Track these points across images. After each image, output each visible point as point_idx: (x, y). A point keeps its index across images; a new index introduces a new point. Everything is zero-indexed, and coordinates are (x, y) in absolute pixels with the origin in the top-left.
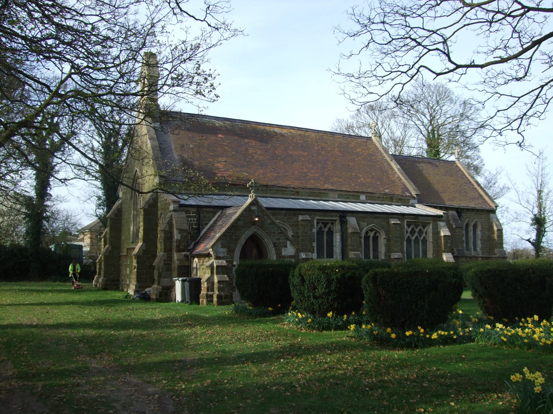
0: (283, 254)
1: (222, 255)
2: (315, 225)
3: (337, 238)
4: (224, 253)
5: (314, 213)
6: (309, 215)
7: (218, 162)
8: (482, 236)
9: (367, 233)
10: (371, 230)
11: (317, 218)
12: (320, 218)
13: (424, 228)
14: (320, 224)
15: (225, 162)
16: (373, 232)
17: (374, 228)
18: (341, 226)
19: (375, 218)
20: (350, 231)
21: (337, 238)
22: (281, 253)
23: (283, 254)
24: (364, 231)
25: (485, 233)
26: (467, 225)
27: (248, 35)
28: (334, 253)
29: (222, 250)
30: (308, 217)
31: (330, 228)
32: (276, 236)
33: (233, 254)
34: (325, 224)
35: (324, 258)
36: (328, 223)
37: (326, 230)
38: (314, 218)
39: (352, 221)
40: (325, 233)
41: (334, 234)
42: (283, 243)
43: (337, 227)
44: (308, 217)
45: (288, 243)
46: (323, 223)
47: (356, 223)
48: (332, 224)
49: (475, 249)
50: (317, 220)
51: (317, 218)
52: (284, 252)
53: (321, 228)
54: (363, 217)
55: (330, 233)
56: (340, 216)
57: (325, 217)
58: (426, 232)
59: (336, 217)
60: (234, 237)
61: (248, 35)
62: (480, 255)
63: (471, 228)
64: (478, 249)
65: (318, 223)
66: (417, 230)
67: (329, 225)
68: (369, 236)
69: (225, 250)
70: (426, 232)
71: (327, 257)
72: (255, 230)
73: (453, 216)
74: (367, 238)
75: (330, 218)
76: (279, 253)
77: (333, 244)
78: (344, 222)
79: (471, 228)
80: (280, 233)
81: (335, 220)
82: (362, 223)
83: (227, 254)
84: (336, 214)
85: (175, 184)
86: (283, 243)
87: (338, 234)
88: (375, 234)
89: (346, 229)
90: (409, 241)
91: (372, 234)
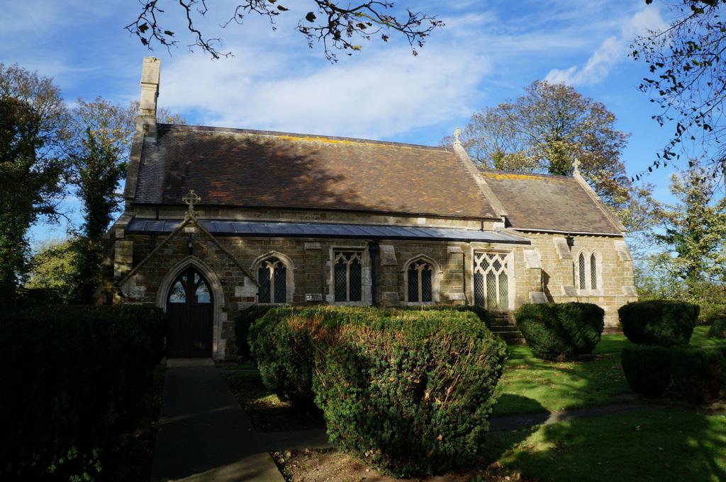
0: (237, 294)
1: (136, 296)
2: (331, 257)
3: (366, 274)
4: (140, 293)
5: (330, 240)
6: (320, 242)
8: (604, 270)
9: (413, 266)
10: (420, 262)
11: (332, 246)
12: (338, 247)
13: (503, 258)
16: (423, 266)
17: (422, 258)
19: (425, 245)
20: (384, 262)
21: (366, 274)
22: (234, 294)
23: (237, 294)
25: (608, 266)
27: (653, 118)
28: (363, 293)
30: (318, 245)
31: (355, 261)
32: (225, 269)
33: (156, 295)
34: (348, 256)
35: (346, 301)
36: (352, 254)
37: (349, 263)
38: (329, 247)
39: (388, 249)
40: (348, 267)
41: (363, 268)
42: (237, 280)
43: (365, 259)
44: (318, 245)
45: (246, 279)
46: (344, 254)
47: (393, 254)
49: (594, 287)
50: (334, 249)
52: (239, 292)
53: (341, 260)
54: (406, 245)
55: (356, 267)
56: (370, 244)
58: (506, 264)
59: (363, 244)
61: (653, 118)
62: (602, 294)
64: (599, 286)
67: (355, 256)
68: (417, 270)
70: (506, 264)
71: (423, 301)
73: (560, 245)
74: (413, 274)
75: (354, 247)
77: (361, 281)
78: (375, 252)
80: (233, 266)
81: (363, 250)
86: (237, 280)
87: (368, 268)
88: (426, 267)
89: (379, 262)
90: (477, 277)
91: (420, 268)
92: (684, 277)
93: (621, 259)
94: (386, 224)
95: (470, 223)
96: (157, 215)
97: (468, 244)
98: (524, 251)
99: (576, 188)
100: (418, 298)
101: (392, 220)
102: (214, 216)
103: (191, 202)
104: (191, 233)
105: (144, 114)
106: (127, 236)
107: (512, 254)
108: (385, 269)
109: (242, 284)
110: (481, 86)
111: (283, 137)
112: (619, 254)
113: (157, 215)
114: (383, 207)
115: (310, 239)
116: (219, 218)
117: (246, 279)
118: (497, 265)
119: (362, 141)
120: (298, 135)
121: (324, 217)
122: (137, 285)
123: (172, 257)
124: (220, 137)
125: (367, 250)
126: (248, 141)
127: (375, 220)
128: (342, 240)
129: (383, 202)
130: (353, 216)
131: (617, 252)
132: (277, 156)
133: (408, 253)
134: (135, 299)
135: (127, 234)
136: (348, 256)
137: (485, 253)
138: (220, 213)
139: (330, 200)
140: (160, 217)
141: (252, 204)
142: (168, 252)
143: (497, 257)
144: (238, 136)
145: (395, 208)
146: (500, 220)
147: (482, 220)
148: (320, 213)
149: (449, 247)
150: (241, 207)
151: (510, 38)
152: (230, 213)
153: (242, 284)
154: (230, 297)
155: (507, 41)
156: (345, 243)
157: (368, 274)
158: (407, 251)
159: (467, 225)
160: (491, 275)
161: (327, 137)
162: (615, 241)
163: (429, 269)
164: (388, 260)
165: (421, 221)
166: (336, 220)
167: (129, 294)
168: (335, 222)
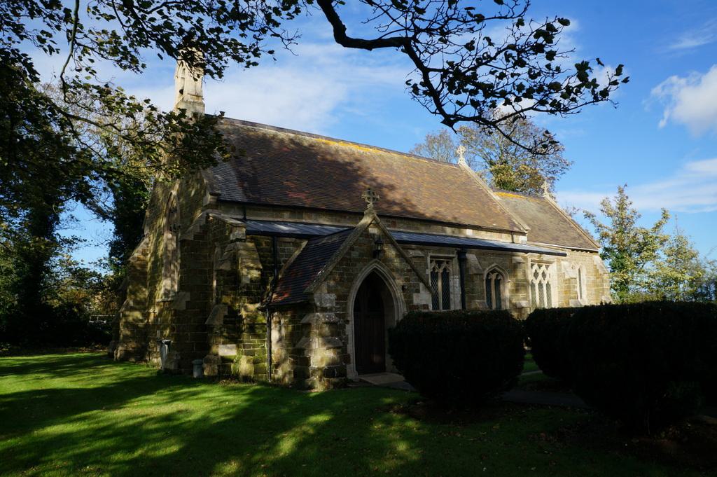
3: (455, 282)
4: (331, 301)
6: (422, 250)
7: (287, 181)
8: (588, 281)
9: (488, 275)
10: (493, 272)
14: (434, 264)
15: (297, 180)
17: (497, 268)
18: (460, 266)
21: (455, 282)
22: (412, 301)
24: (486, 273)
26: (488, 281)
29: (328, 296)
31: (445, 269)
33: (346, 304)
34: (439, 263)
36: (442, 262)
37: (441, 271)
40: (440, 275)
43: (454, 267)
44: (419, 253)
46: (437, 262)
47: (477, 262)
48: (447, 263)
50: (431, 257)
51: (430, 254)
55: (446, 276)
56: (459, 253)
57: (440, 253)
59: (453, 253)
60: (345, 277)
63: (493, 283)
65: (431, 262)
66: (540, 277)
67: (444, 265)
69: (333, 297)
72: (375, 266)
75: (446, 255)
76: (409, 301)
77: (449, 290)
78: (462, 260)
79: (493, 283)
81: (452, 258)
82: (483, 262)
83: (337, 304)
84: (452, 249)
85: (162, 39)
88: (497, 276)
89: (467, 270)
91: (493, 277)
92: (616, 290)
93: (601, 272)
94: (444, 234)
95: (504, 235)
96: (245, 215)
97: (526, 255)
98: (562, 262)
99: (550, 208)
100: (438, 306)
101: (449, 230)
102: (299, 219)
103: (371, 200)
104: (374, 234)
105: (192, 101)
106: (248, 236)
107: (555, 263)
108: (475, 277)
109: (418, 291)
110: (334, 112)
111: (320, 140)
112: (598, 268)
113: (245, 215)
114: (439, 217)
115: (414, 246)
116: (304, 221)
117: (421, 285)
118: (544, 275)
119: (388, 151)
120: (333, 140)
121: (394, 225)
122: (328, 293)
123: (357, 260)
124: (264, 135)
125: (456, 258)
126: (292, 141)
127: (436, 230)
128: (437, 248)
129: (437, 212)
130: (416, 224)
131: (596, 266)
132: (327, 160)
133: (486, 262)
134: (326, 308)
135: (249, 235)
136: (439, 263)
137: (537, 264)
138: (304, 216)
139: (396, 208)
140: (247, 218)
141: (332, 208)
142: (355, 254)
143: (543, 268)
144: (282, 135)
145: (449, 218)
146: (524, 234)
147: (512, 233)
148: (391, 221)
149: (515, 257)
150: (323, 210)
151: (367, 69)
152: (313, 215)
153: (418, 291)
154: (409, 301)
155: (364, 71)
156: (439, 252)
157: (458, 282)
158: (485, 260)
159: (501, 238)
160: (540, 285)
161: (358, 144)
162: (594, 256)
163: (499, 278)
164: (476, 269)
165: (469, 233)
166: (404, 228)
167: (321, 303)
168: (404, 230)
